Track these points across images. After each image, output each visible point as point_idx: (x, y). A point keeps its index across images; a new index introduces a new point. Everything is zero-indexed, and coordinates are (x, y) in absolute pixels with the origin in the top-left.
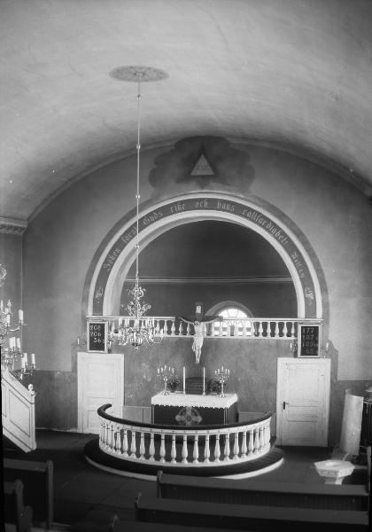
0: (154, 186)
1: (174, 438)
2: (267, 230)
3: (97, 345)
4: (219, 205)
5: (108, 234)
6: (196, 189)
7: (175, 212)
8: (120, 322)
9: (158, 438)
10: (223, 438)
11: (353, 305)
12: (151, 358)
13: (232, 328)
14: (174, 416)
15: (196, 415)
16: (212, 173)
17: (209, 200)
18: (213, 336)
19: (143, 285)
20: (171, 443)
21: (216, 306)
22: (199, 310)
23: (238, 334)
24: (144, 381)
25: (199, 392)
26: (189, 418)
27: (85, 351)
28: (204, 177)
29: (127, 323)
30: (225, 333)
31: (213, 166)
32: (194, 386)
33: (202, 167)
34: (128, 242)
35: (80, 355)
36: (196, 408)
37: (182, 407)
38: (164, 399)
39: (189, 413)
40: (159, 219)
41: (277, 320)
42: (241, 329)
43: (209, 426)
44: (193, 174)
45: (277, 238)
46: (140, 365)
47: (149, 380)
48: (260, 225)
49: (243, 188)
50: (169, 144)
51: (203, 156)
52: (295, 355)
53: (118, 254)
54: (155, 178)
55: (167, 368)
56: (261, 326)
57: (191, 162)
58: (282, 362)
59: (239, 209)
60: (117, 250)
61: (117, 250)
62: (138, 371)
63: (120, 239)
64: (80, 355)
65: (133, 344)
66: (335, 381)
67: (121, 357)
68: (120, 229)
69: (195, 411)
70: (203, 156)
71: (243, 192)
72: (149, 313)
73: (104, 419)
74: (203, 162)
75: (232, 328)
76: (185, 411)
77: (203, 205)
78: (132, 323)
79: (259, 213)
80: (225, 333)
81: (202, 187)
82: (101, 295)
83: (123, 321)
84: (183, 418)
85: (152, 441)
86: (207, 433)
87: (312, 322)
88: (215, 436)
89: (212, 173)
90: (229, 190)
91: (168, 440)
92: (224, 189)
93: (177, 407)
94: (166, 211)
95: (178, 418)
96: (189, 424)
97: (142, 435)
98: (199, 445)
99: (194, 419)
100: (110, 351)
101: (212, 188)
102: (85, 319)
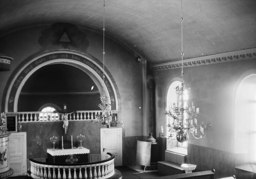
2: (95, 70)
6: (62, 48)
8: (96, 114)
9: (62, 170)
11: (130, 104)
13: (49, 117)
14: (65, 160)
15: (75, 158)
16: (69, 41)
18: (39, 121)
20: (79, 172)
22: (65, 107)
23: (52, 119)
24: (38, 145)
25: (70, 147)
26: (72, 160)
29: (99, 114)
30: (46, 119)
32: (68, 147)
33: (65, 38)
36: (75, 155)
37: (68, 155)
39: (72, 158)
41: (27, 113)
42: (53, 117)
44: (60, 41)
45: (99, 74)
46: (35, 136)
47: (40, 144)
49: (84, 50)
51: (65, 33)
52: (108, 127)
55: (54, 137)
58: (102, 130)
61: (22, 77)
62: (34, 140)
65: (103, 124)
66: (124, 137)
67: (25, 134)
69: (75, 156)
70: (65, 33)
71: (84, 52)
73: (36, 164)
74: (65, 36)
75: (49, 117)
76: (70, 157)
77: (65, 56)
78: (101, 113)
79: (91, 62)
80: (46, 119)
81: (65, 48)
82: (12, 101)
83: (98, 113)
84: (69, 160)
88: (89, 168)
89: (69, 41)
90: (78, 50)
91: (83, 170)
93: (66, 155)
94: (47, 58)
95: (67, 161)
96: (72, 163)
97: (59, 170)
99: (74, 160)
100: (18, 131)
101: (69, 49)
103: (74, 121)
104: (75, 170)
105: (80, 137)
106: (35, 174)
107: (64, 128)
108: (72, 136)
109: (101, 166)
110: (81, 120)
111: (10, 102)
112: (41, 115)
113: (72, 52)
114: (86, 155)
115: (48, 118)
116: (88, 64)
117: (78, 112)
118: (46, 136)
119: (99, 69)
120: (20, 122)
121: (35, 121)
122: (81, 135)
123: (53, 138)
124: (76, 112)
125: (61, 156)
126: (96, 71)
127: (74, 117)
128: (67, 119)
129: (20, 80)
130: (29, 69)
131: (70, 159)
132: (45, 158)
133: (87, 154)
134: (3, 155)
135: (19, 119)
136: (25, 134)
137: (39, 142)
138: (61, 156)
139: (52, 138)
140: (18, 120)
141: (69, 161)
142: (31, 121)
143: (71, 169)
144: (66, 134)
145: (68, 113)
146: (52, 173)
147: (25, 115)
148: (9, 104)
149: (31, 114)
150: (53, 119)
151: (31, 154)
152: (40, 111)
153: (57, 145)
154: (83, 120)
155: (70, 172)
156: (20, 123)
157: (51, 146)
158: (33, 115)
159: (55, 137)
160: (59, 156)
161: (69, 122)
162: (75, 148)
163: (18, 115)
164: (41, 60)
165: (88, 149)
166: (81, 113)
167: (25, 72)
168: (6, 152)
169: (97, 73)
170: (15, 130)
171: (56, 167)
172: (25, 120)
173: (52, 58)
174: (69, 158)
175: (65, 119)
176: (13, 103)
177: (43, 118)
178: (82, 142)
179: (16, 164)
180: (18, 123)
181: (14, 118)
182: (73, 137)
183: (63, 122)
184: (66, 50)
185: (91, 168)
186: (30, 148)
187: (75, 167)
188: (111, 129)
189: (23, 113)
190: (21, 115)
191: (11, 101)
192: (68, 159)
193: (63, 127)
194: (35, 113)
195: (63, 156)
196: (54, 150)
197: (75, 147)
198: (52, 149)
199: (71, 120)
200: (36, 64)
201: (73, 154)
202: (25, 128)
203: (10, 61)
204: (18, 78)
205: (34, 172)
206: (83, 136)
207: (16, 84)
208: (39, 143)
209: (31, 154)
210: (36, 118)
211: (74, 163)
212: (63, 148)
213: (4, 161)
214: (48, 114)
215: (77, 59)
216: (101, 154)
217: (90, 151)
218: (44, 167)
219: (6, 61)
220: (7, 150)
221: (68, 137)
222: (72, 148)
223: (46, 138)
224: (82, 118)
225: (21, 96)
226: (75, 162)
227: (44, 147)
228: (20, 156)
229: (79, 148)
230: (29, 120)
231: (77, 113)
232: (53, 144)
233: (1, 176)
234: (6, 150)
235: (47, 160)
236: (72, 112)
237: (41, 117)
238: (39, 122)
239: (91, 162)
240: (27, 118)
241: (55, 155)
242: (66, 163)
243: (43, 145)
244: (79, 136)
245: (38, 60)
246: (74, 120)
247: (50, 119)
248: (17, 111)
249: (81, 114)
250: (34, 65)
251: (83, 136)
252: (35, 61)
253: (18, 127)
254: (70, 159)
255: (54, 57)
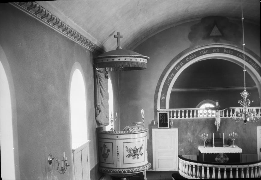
0: (191, 41)
1: (225, 169)
3: (163, 123)
4: (225, 50)
5: (167, 66)
7: (202, 55)
10: (250, 168)
12: (192, 129)
15: (226, 157)
16: (221, 35)
17: (220, 48)
19: (247, 91)
20: (224, 172)
21: (203, 101)
25: (221, 145)
26: (222, 159)
27: (157, 128)
28: (217, 37)
31: (221, 30)
32: (219, 144)
33: (215, 32)
34: (178, 70)
35: (154, 130)
36: (226, 153)
37: (218, 154)
38: (204, 150)
40: (194, 58)
41: (187, 109)
43: (232, 163)
46: (187, 133)
47: (191, 141)
48: (193, 59)
50: (198, 20)
51: (215, 26)
53: (173, 76)
54: (191, 37)
55: (234, 134)
56: (179, 112)
57: (209, 29)
59: (235, 53)
60: (173, 74)
61: (173, 74)
62: (186, 137)
63: (174, 68)
64: (154, 130)
67: (176, 130)
68: (174, 63)
69: (225, 155)
70: (215, 26)
72: (252, 105)
74: (216, 29)
76: (220, 155)
77: (217, 51)
82: (164, 98)
84: (219, 159)
85: (219, 172)
86: (231, 167)
87: (162, 111)
92: (228, 43)
94: (198, 54)
95: (216, 159)
96: (222, 162)
98: (221, 172)
99: (224, 159)
100: (170, 127)
101: (221, 43)
102: (156, 111)
103: (227, 118)
104: (219, 169)
105: (232, 135)
106: (184, 171)
107: (216, 125)
108: (224, 134)
109: (254, 168)
110: (183, 118)
111: (162, 99)
112: (200, 111)
113: (212, 46)
114: (237, 155)
115: (207, 114)
116: (242, 57)
117: (231, 108)
118: (197, 133)
119: (179, 63)
120: (171, 118)
121: (195, 118)
122: (233, 133)
123: (204, 135)
124: (229, 108)
125: (210, 154)
126: (251, 64)
127: (228, 114)
128: (219, 116)
129: (171, 77)
130: (180, 66)
131: (220, 157)
132: (196, 155)
133: (239, 154)
134: (139, 150)
135: (171, 115)
136: (176, 130)
137: (190, 139)
138: (210, 154)
139: (203, 135)
140: (170, 117)
141: (219, 160)
142: (191, 118)
143: (221, 169)
144: (218, 132)
145: (221, 109)
146: (201, 171)
147: (177, 112)
148: (161, 100)
149: (183, 110)
150: (201, 116)
151: (182, 150)
152: (199, 107)
153: (208, 142)
154: (189, 118)
155: (214, 172)
156: (172, 119)
157: (202, 143)
158: (193, 112)
159: (235, 134)
160: (208, 154)
161: (221, 119)
162: (227, 146)
163: (170, 112)
164: (191, 56)
165: (241, 148)
166: (191, 110)
167: (176, 69)
168: (143, 147)
169: (253, 66)
170: (167, 126)
171: (206, 165)
172: (177, 117)
173: (203, 53)
174: (219, 157)
175: (217, 116)
176: (165, 100)
177: (203, 114)
178: (234, 140)
179: (163, 159)
180: (170, 120)
181: (166, 114)
182: (224, 134)
183: (215, 119)
184: (217, 44)
185: (237, 170)
186: (182, 144)
187: (226, 167)
188: (160, 129)
189: (175, 110)
190: (173, 112)
191: (163, 98)
192: (218, 157)
193: (215, 125)
194: (195, 109)
195: (213, 154)
196: (205, 148)
197: (228, 146)
198: (203, 146)
199: (224, 117)
200: (187, 60)
201: (224, 153)
202: (177, 125)
203: (146, 60)
204: (169, 75)
205: (183, 168)
206: (236, 134)
207: (168, 81)
208: (190, 140)
209: (182, 150)
210: (195, 114)
211: (224, 162)
212: (214, 146)
213: (140, 155)
214: (206, 110)
215: (230, 52)
216: (257, 155)
217: (243, 151)
218: (193, 165)
219: (140, 60)
220: (143, 145)
221: (220, 134)
222: (224, 146)
223: (197, 135)
224: (224, 116)
225: (172, 93)
226: (225, 161)
227: (196, 144)
228: (172, 152)
229: (231, 146)
230: (181, 116)
231: (230, 110)
232: (204, 141)
233: (137, 169)
234: (142, 145)
235: (198, 157)
236: (225, 109)
237: (201, 114)
238: (198, 119)
239: (243, 162)
240: (179, 115)
241: (204, 153)
242: (216, 161)
243: (195, 142)
244: (203, 135)
245: (189, 56)
246: (228, 117)
247: (198, 116)
248: (160, 108)
249: (183, 112)
250: (185, 61)
251: (236, 134)
252: (186, 57)
253: (170, 123)
254: (220, 157)
255: (205, 53)
